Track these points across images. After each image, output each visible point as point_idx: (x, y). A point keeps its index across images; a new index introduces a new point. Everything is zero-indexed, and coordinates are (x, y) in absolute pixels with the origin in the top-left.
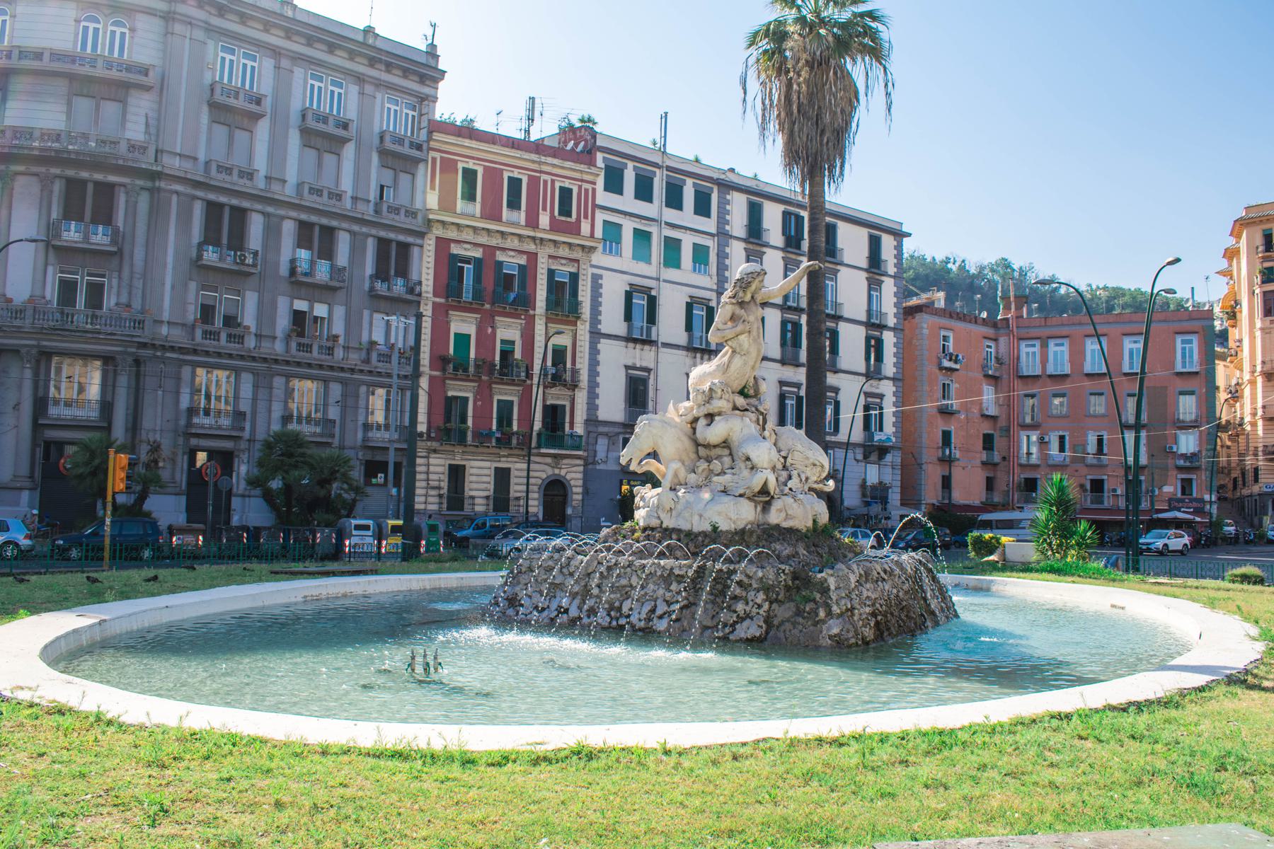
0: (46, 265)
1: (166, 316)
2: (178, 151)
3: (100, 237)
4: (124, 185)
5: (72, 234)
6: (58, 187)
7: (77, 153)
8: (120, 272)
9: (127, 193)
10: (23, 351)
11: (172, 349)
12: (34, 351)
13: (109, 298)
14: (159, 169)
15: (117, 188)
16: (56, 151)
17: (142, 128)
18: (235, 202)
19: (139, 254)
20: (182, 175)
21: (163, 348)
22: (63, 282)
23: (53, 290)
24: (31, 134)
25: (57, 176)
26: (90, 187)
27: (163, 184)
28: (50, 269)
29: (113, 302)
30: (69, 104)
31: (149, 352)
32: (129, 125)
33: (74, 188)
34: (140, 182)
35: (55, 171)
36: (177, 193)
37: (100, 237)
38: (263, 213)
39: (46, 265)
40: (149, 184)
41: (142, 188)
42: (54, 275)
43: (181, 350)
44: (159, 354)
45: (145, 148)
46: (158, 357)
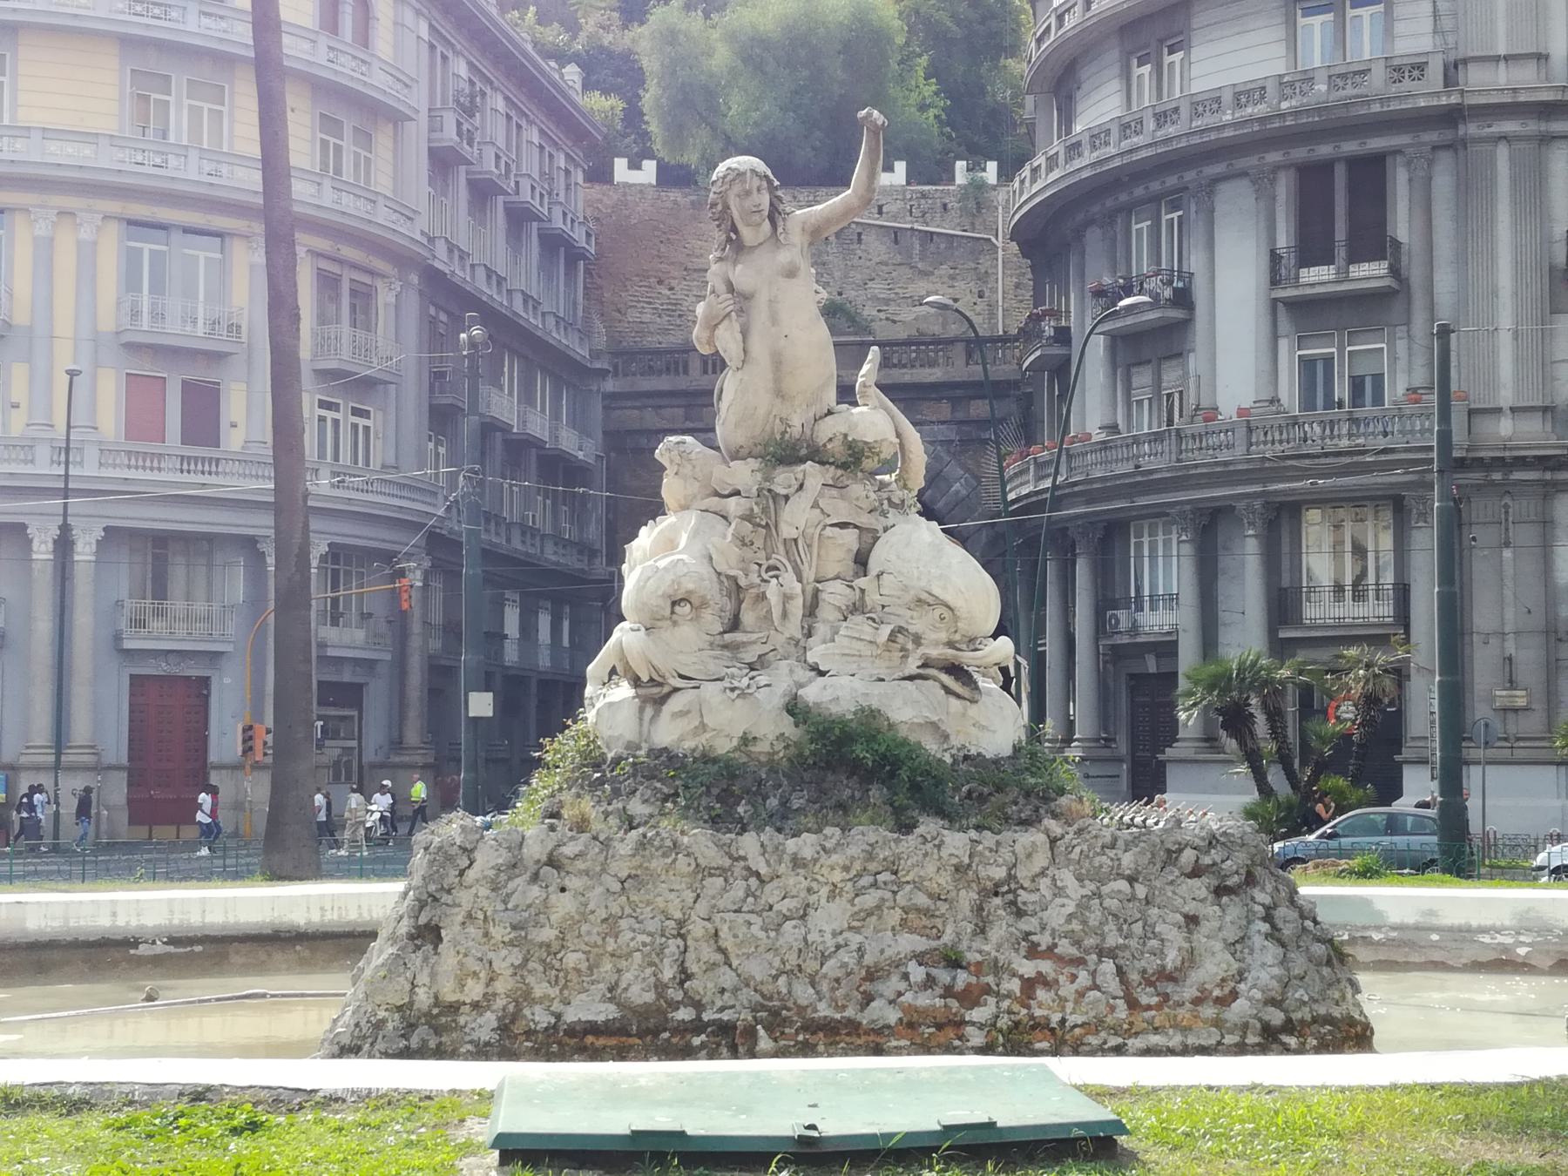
0: (1275, 337)
1: (1506, 398)
2: (1502, 51)
3: (1371, 273)
4: (1397, 152)
5: (1318, 277)
6: (1284, 188)
7: (1296, 113)
8: (1408, 323)
9: (1409, 163)
10: (1241, 505)
11: (1522, 463)
12: (1258, 504)
13: (1393, 383)
14: (1454, 99)
15: (1389, 160)
16: (1262, 120)
17: (1427, 25)
18: (1350, 147)
19: (1444, 282)
20: (1507, 98)
21: (1499, 463)
22: (1307, 364)
23: (1291, 385)
24: (1218, 100)
25: (1277, 168)
26: (1340, 173)
27: (1472, 129)
28: (1283, 344)
29: (1401, 389)
30: (1291, 24)
31: (1476, 477)
32: (1400, 28)
33: (1312, 183)
34: (1431, 137)
35: (1274, 157)
36: (1503, 138)
37: (1371, 273)
38: (120, 219)
39: (1275, 337)
40: (1448, 135)
41: (1435, 148)
42: (1291, 353)
43: (1543, 462)
44: (1497, 476)
45: (1421, 67)
46: (1493, 483)
